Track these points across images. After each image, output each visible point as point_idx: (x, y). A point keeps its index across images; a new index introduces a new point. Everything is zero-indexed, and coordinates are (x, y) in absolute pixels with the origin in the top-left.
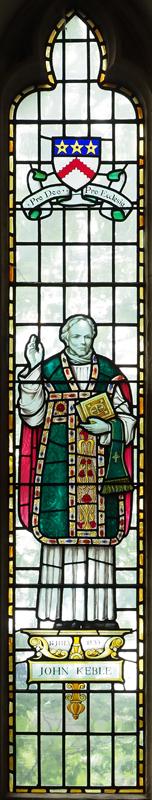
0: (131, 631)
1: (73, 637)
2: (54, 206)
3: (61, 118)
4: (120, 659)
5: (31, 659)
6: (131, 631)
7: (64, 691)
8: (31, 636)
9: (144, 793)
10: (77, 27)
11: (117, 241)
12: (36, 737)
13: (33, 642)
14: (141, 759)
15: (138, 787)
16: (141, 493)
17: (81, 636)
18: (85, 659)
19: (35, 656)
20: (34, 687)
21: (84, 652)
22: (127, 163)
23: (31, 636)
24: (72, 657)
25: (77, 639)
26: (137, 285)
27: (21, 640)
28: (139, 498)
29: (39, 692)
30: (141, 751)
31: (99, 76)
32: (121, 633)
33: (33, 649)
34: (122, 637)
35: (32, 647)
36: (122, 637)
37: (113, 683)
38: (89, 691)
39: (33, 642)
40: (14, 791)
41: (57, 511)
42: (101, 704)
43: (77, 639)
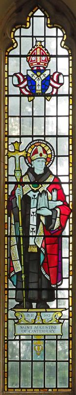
0: (66, 309)
1: (37, 312)
2: (56, 155)
3: (56, 115)
5: (18, 143)
6: (66, 309)
8: (16, 312)
9: (50, 230)
10: (39, 12)
11: (55, 38)
12: (31, 360)
13: (17, 314)
14: (6, 66)
15: (69, 388)
16: (71, 222)
17: (41, 312)
18: (43, 324)
19: (18, 322)
20: (17, 338)
21: (42, 320)
23: (16, 312)
25: (39, 314)
26: (69, 95)
27: (11, 314)
28: (70, 224)
30: (6, 104)
31: (8, 186)
32: (60, 310)
33: (17, 319)
34: (61, 312)
35: (16, 317)
36: (61, 312)
37: (57, 335)
38: (45, 340)
39: (17, 314)
40: (8, 391)
41: (43, 289)
42: (14, 346)
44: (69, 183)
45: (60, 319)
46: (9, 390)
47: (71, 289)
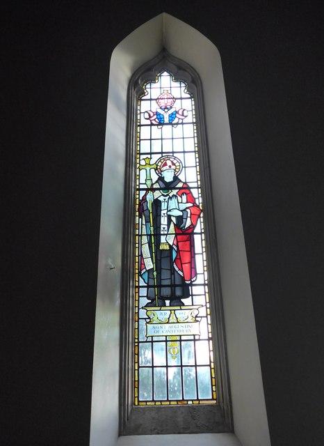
1: (171, 310)
4: (198, 321)
7: (166, 341)
17: (175, 310)
18: (178, 322)
20: (150, 339)
22: (146, 342)
24: (170, 322)
25: (173, 312)
29: (152, 342)
37: (194, 335)
40: (138, 404)
43: (173, 312)
44: (198, 188)
45: (196, 317)
46: (140, 403)
47: (207, 285)
